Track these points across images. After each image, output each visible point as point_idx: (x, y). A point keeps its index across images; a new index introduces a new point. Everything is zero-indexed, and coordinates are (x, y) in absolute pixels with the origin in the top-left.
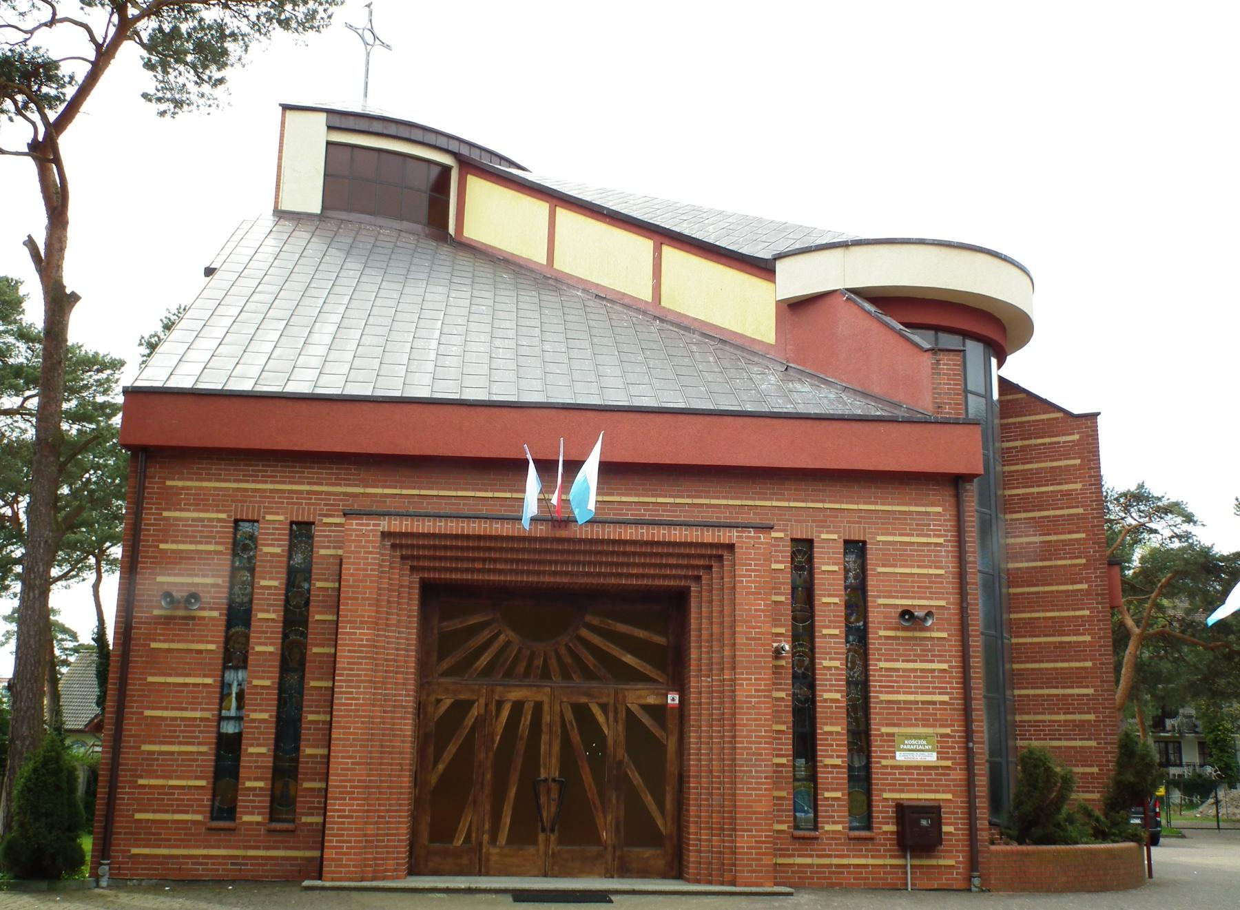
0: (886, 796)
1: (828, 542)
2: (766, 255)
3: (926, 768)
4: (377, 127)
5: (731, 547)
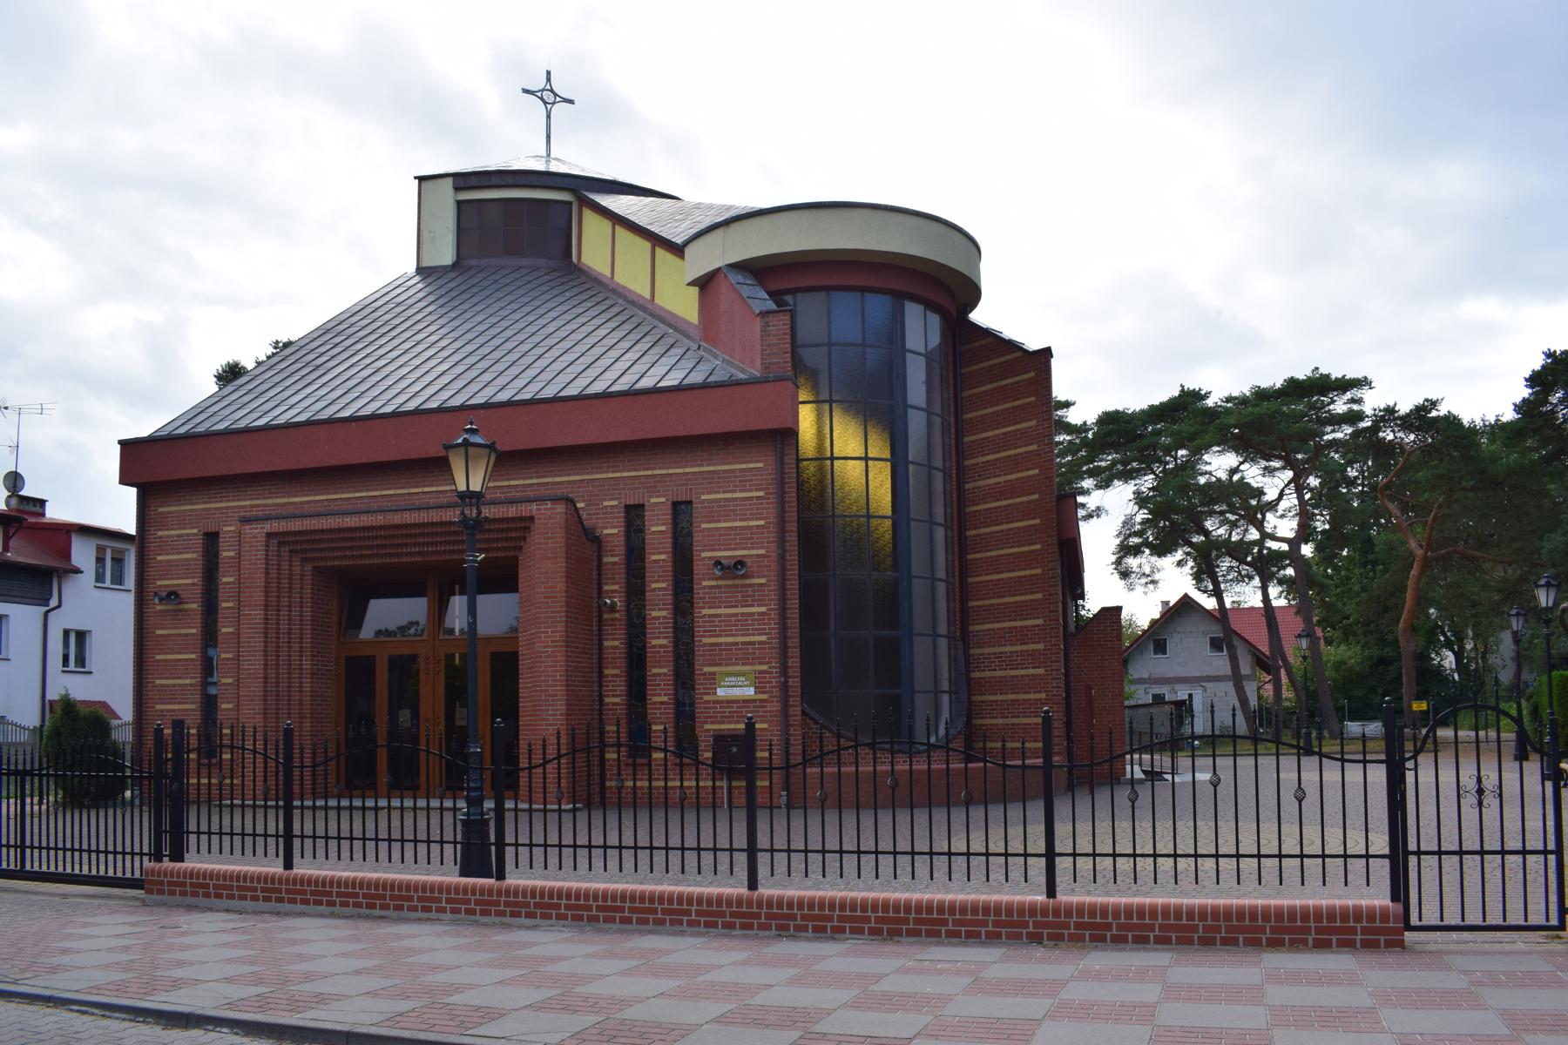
0: (708, 728)
1: (658, 502)
2: (679, 240)
3: (745, 701)
4: (495, 180)
5: (532, 519)
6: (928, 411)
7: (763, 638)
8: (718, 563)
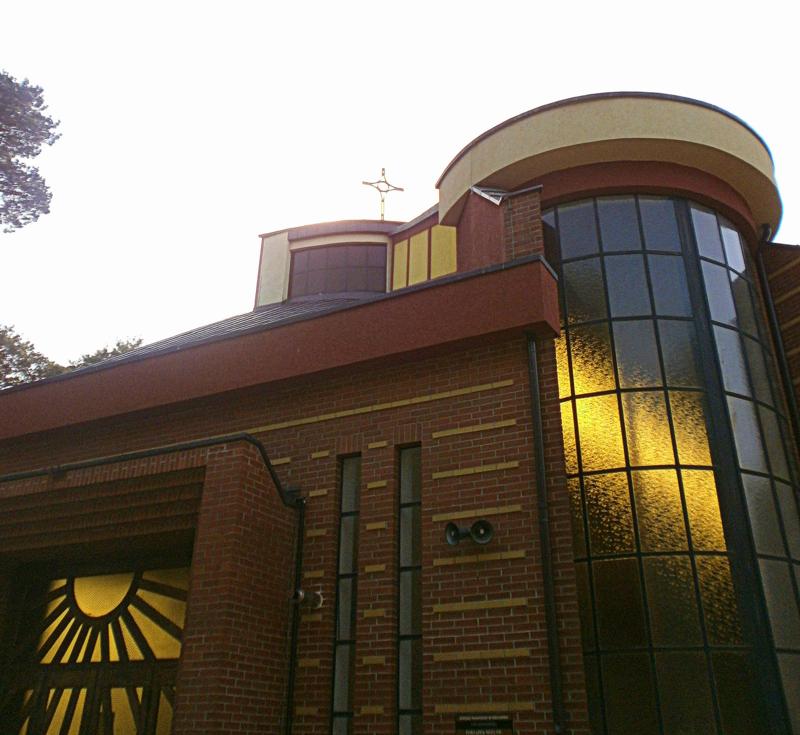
6: (738, 327)
7: (525, 652)
8: (451, 525)
